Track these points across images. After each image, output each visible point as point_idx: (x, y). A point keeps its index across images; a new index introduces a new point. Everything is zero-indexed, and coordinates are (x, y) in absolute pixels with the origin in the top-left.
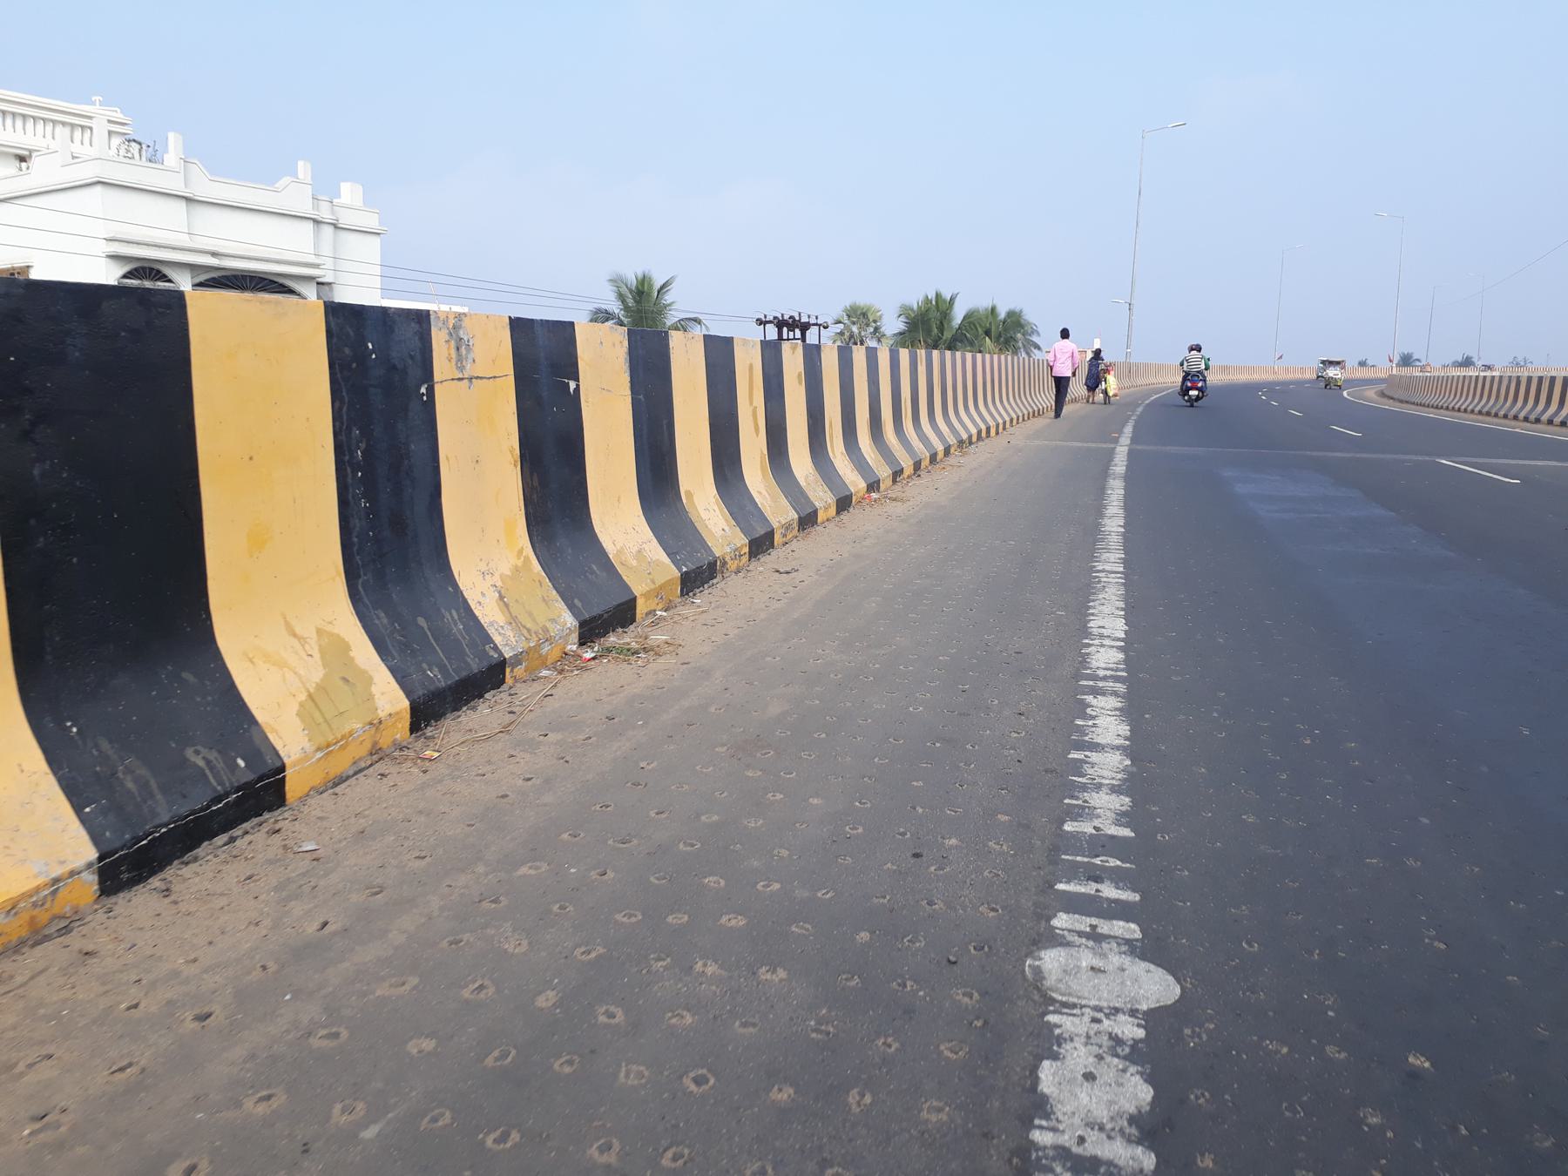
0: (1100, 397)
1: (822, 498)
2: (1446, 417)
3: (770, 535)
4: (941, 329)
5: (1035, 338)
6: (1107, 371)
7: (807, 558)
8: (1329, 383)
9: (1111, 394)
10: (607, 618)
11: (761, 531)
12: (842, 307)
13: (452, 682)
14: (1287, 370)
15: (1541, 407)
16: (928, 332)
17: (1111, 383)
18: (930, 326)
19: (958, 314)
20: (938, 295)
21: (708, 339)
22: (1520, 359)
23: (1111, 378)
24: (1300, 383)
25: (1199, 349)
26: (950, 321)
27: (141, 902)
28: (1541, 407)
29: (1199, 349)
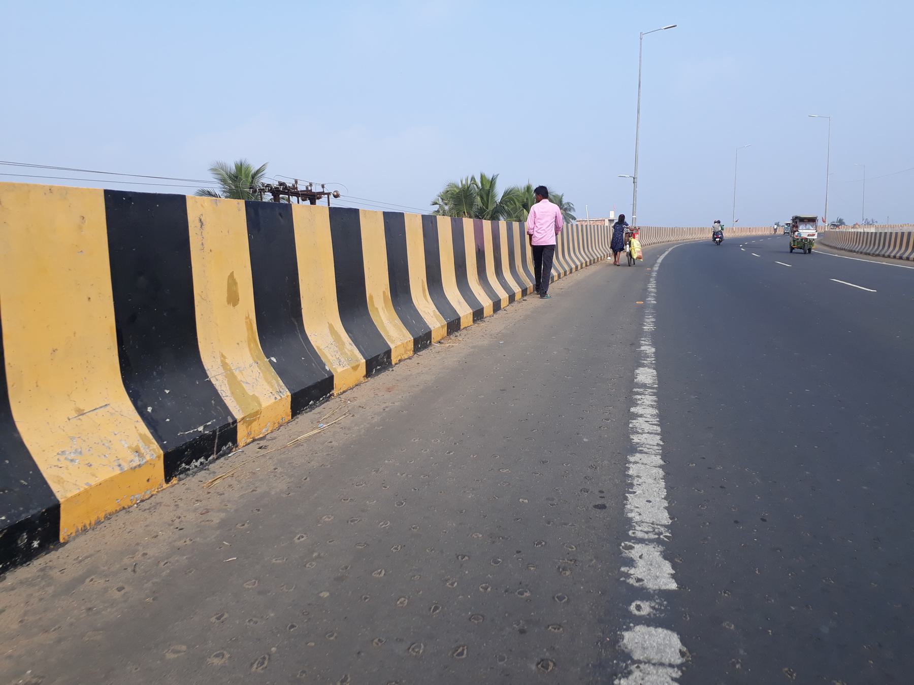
0: (622, 255)
1: (464, 311)
2: (847, 256)
3: (428, 335)
4: (486, 203)
5: (572, 213)
6: (632, 234)
7: (473, 336)
8: (804, 246)
9: (635, 256)
10: (378, 362)
11: (421, 333)
12: (441, 189)
13: (311, 391)
14: (742, 230)
15: (897, 249)
16: (471, 204)
17: (636, 247)
18: (471, 201)
19: (499, 193)
20: (483, 177)
21: (336, 214)
22: (869, 220)
23: (635, 242)
24: (764, 237)
25: (719, 222)
26: (493, 196)
27: (304, 418)
28: (897, 249)
29: (841, 222)
